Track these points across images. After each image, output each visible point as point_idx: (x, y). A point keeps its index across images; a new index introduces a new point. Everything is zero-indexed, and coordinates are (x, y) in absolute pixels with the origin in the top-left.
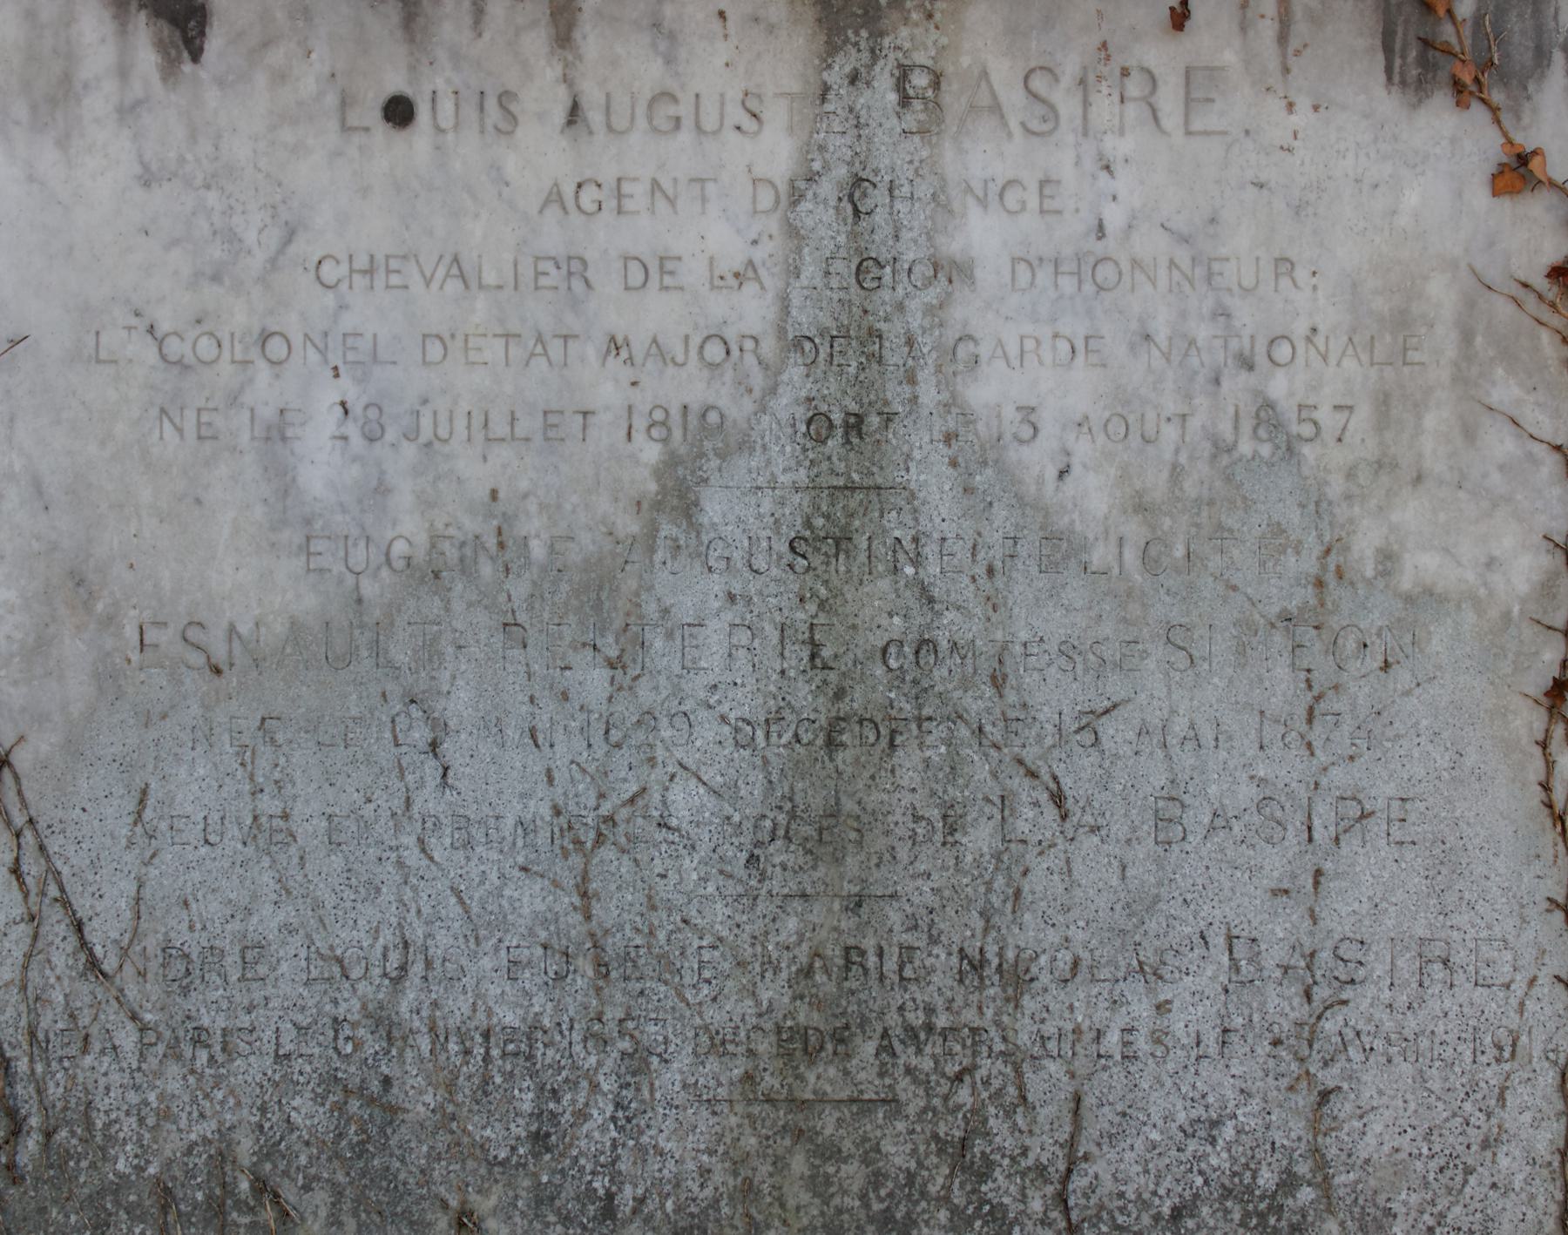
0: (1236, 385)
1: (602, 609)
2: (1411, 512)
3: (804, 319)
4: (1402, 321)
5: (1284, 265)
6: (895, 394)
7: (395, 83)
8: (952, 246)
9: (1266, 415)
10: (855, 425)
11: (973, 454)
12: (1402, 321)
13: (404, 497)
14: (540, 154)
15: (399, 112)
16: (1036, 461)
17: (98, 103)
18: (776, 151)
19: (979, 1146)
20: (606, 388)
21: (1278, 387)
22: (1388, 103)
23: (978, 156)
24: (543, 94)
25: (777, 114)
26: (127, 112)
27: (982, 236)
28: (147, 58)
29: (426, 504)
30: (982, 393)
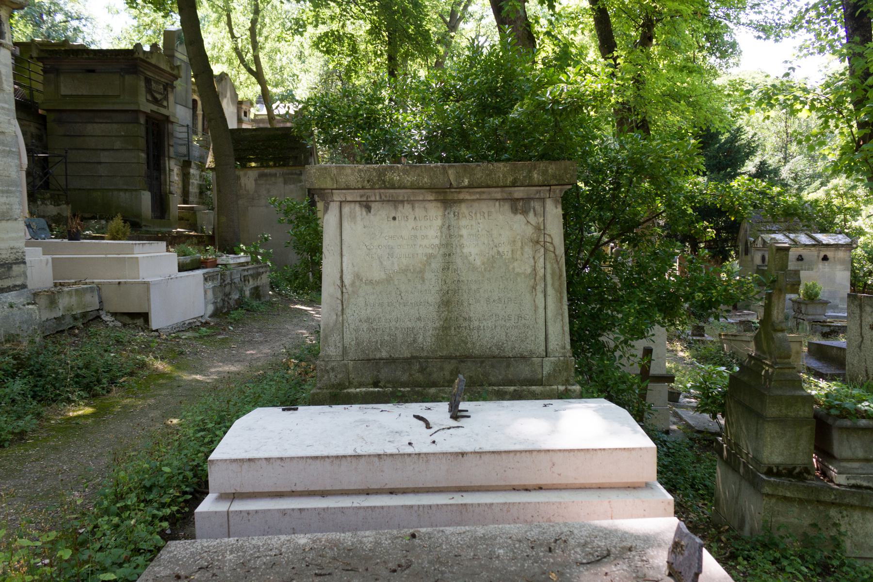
0: (495, 250)
1: (421, 274)
2: (516, 264)
3: (444, 242)
4: (514, 241)
5: (500, 235)
6: (454, 251)
7: (393, 215)
8: (461, 233)
9: (498, 252)
10: (450, 255)
11: (465, 257)
12: (514, 241)
13: (396, 265)
14: (411, 223)
15: (394, 218)
16: (471, 258)
17: (359, 218)
18: (439, 222)
19: (645, 317)
20: (420, 251)
21: (501, 249)
22: (512, 215)
23: (463, 222)
24: (411, 217)
25: (439, 218)
26: (362, 219)
27: (464, 232)
28: (364, 213)
29: (398, 265)
30: (465, 250)
